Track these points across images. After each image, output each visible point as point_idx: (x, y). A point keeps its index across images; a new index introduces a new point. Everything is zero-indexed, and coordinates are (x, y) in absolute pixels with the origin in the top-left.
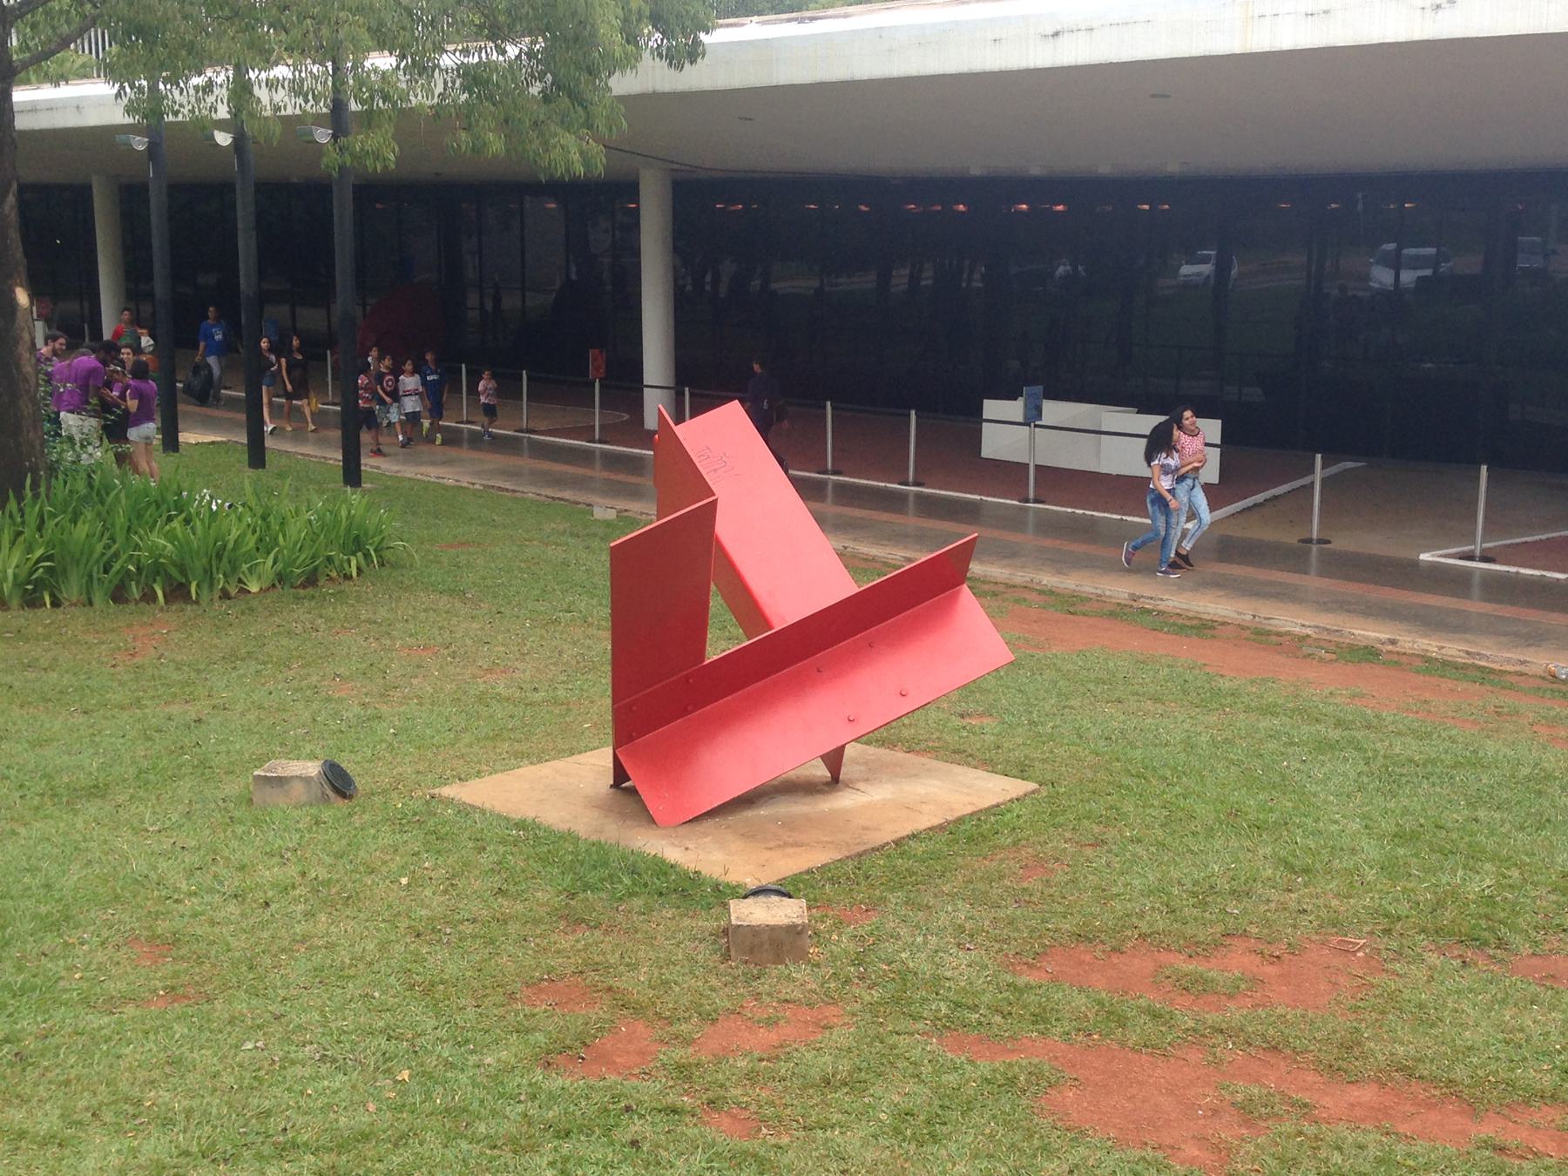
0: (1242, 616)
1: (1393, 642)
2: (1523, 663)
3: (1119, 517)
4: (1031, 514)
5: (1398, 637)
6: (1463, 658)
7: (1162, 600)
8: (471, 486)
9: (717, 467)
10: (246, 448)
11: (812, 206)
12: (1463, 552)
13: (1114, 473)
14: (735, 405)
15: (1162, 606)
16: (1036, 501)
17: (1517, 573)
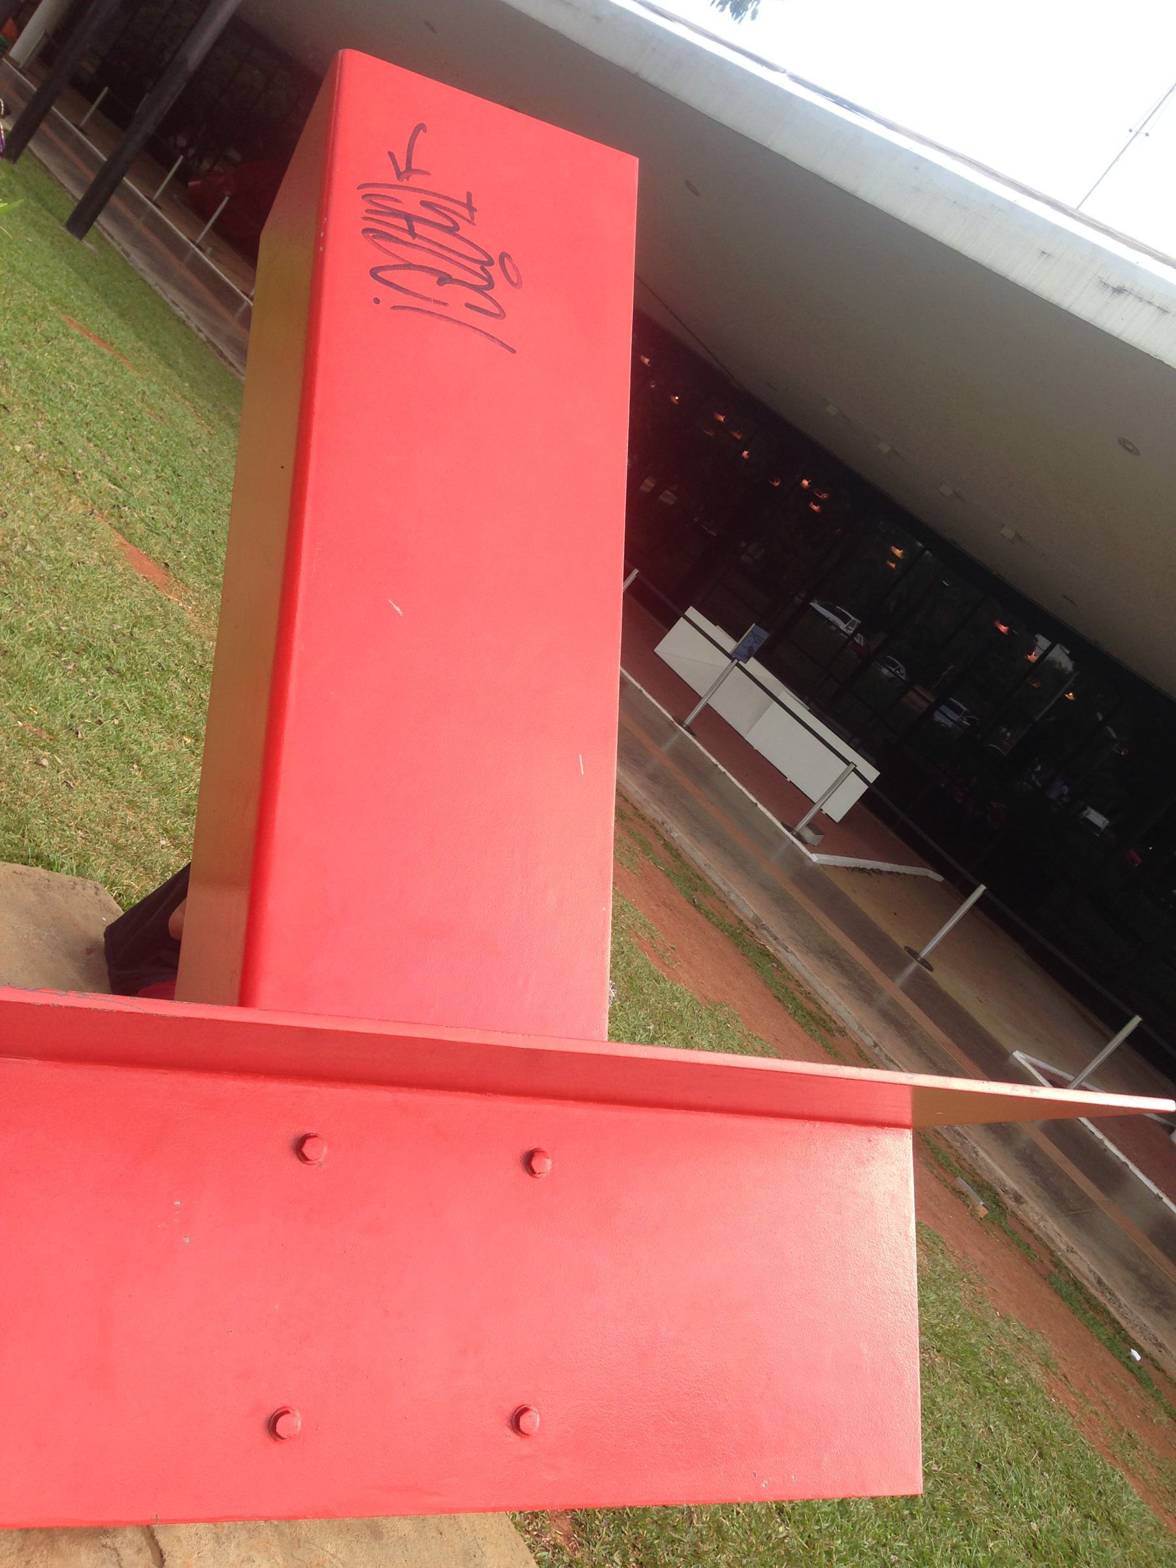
0: (862, 1035)
1: (1018, 1199)
2: (1160, 1346)
3: (755, 801)
4: (675, 738)
5: (1026, 1197)
6: (1090, 1283)
7: (786, 948)
8: (196, 331)
9: (458, 273)
10: (76, 204)
11: (398, 609)
12: (1053, 1074)
13: (755, 748)
14: (633, 163)
15: (782, 955)
16: (688, 729)
17: (1101, 1141)
